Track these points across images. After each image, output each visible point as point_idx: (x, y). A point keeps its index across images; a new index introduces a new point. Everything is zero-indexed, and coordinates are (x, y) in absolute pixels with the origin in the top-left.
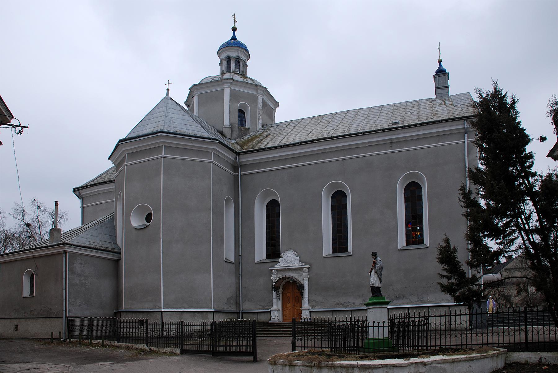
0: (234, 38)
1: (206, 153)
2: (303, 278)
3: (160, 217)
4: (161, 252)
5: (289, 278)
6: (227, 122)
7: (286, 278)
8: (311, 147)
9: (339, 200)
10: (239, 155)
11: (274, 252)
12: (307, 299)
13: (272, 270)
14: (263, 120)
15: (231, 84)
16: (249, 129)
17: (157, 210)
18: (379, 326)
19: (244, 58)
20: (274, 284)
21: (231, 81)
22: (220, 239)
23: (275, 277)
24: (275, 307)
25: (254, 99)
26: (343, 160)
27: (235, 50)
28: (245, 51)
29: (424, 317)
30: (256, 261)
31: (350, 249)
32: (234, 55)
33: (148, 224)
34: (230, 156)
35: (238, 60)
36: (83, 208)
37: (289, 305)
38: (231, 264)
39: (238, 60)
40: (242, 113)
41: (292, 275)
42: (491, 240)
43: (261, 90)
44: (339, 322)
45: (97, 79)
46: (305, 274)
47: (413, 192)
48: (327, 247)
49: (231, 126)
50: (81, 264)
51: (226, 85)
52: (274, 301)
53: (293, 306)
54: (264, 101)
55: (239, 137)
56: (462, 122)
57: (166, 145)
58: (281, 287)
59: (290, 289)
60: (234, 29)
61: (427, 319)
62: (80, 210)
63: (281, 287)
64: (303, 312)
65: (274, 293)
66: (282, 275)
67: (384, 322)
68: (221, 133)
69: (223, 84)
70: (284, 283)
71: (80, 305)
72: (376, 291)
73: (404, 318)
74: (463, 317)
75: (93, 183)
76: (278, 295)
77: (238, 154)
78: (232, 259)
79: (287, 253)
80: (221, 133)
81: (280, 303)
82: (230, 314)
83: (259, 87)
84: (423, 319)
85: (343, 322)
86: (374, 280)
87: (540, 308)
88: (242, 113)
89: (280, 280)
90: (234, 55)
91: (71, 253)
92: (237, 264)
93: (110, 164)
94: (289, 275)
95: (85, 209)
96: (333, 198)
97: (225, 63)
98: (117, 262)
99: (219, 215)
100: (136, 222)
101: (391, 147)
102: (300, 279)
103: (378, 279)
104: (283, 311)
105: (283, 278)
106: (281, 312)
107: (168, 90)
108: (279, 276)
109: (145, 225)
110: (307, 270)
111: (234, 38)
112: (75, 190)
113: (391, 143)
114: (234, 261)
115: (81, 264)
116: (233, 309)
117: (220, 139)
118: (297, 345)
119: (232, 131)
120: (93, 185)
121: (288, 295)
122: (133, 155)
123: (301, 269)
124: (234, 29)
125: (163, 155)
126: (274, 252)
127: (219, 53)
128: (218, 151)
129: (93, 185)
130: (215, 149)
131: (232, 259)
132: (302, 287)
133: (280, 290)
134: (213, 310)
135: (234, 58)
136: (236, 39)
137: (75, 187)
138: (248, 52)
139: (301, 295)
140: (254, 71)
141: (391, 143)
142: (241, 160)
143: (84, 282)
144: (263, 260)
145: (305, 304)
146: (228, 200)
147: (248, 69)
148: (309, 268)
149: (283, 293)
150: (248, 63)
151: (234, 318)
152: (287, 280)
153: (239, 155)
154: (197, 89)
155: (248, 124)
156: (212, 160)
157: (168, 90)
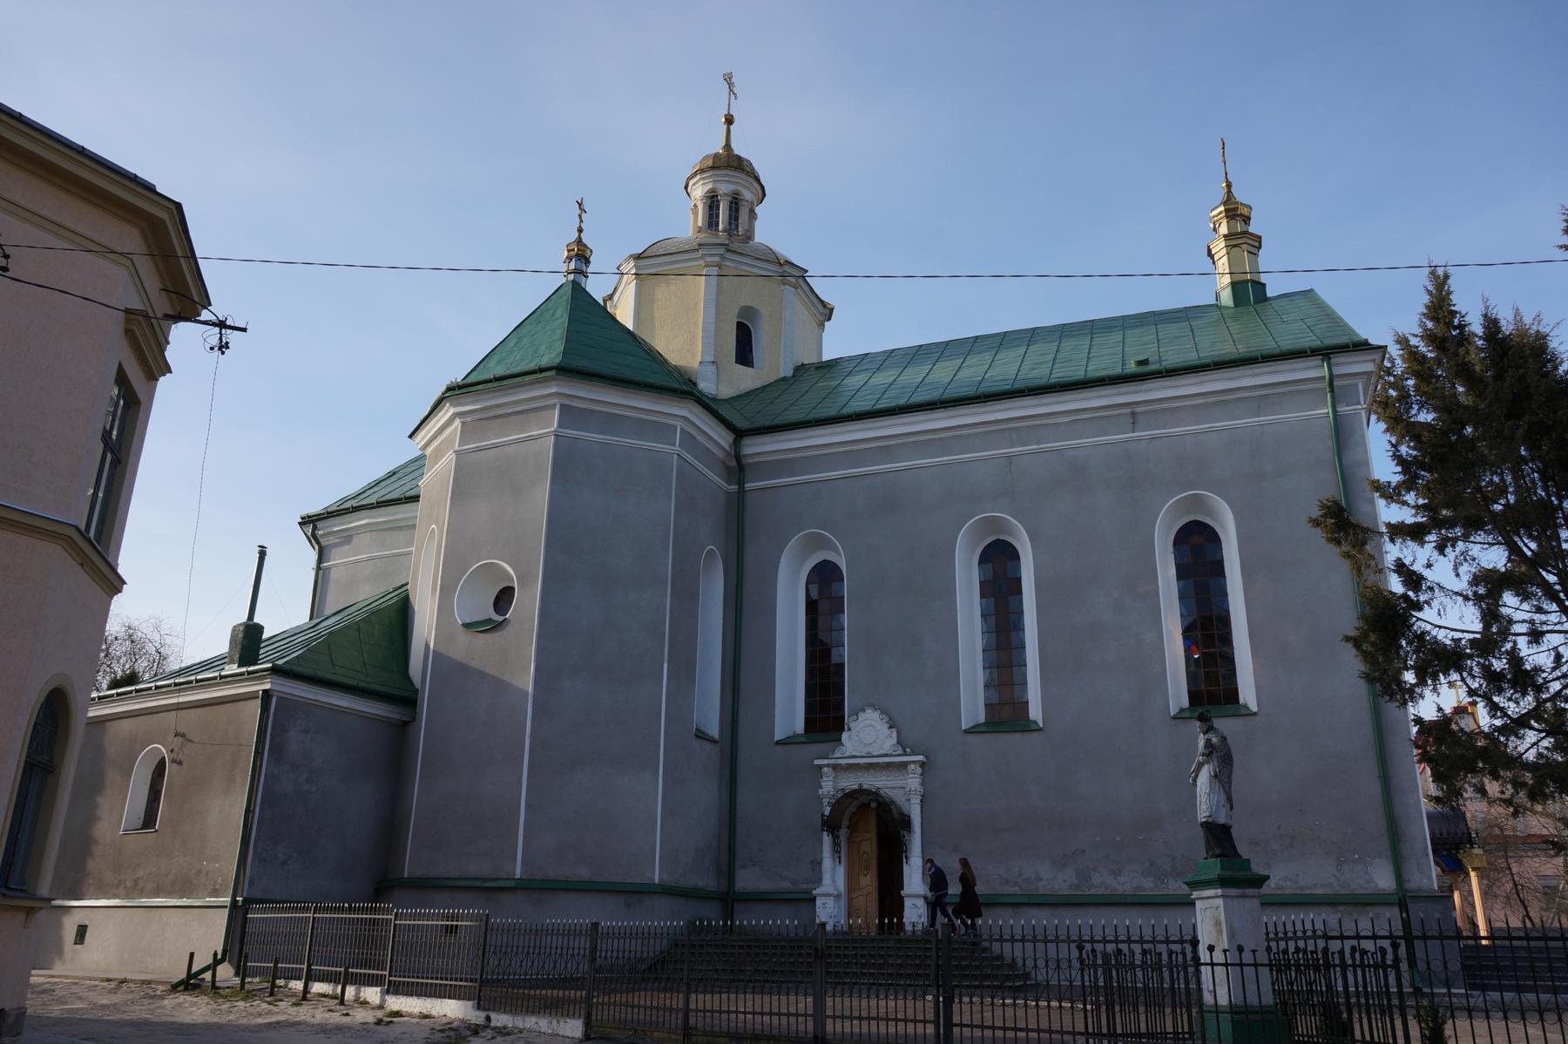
2: (905, 790)
7: (860, 792)
11: (826, 715)
13: (820, 767)
19: (747, 195)
20: (827, 811)
23: (829, 786)
26: (1009, 457)
30: (777, 738)
31: (1248, 693)
33: (501, 618)
34: (723, 438)
41: (878, 784)
42: (1435, 690)
44: (1105, 941)
46: (913, 782)
47: (1198, 549)
48: (972, 704)
52: (827, 862)
56: (1316, 361)
58: (845, 823)
59: (874, 827)
62: (313, 573)
63: (845, 823)
65: (827, 839)
66: (850, 782)
70: (853, 808)
71: (284, 863)
73: (1286, 939)
75: (354, 503)
78: (714, 731)
79: (862, 716)
81: (841, 872)
85: (1116, 941)
92: (730, 743)
96: (984, 559)
98: (401, 733)
99: (687, 597)
101: (1134, 426)
102: (898, 797)
105: (854, 792)
106: (843, 903)
110: (919, 770)
112: (306, 521)
114: (716, 736)
115: (306, 732)
116: (708, 882)
118: (956, 1020)
120: (347, 511)
123: (904, 765)
126: (826, 715)
128: (693, 424)
129: (347, 511)
130: (686, 418)
131: (714, 731)
132: (906, 823)
133: (843, 833)
138: (757, 180)
140: (772, 229)
141: (1134, 416)
143: (306, 787)
144: (795, 736)
147: (757, 224)
148: (922, 764)
149: (849, 839)
150: (758, 210)
151: (711, 915)
152: (864, 799)
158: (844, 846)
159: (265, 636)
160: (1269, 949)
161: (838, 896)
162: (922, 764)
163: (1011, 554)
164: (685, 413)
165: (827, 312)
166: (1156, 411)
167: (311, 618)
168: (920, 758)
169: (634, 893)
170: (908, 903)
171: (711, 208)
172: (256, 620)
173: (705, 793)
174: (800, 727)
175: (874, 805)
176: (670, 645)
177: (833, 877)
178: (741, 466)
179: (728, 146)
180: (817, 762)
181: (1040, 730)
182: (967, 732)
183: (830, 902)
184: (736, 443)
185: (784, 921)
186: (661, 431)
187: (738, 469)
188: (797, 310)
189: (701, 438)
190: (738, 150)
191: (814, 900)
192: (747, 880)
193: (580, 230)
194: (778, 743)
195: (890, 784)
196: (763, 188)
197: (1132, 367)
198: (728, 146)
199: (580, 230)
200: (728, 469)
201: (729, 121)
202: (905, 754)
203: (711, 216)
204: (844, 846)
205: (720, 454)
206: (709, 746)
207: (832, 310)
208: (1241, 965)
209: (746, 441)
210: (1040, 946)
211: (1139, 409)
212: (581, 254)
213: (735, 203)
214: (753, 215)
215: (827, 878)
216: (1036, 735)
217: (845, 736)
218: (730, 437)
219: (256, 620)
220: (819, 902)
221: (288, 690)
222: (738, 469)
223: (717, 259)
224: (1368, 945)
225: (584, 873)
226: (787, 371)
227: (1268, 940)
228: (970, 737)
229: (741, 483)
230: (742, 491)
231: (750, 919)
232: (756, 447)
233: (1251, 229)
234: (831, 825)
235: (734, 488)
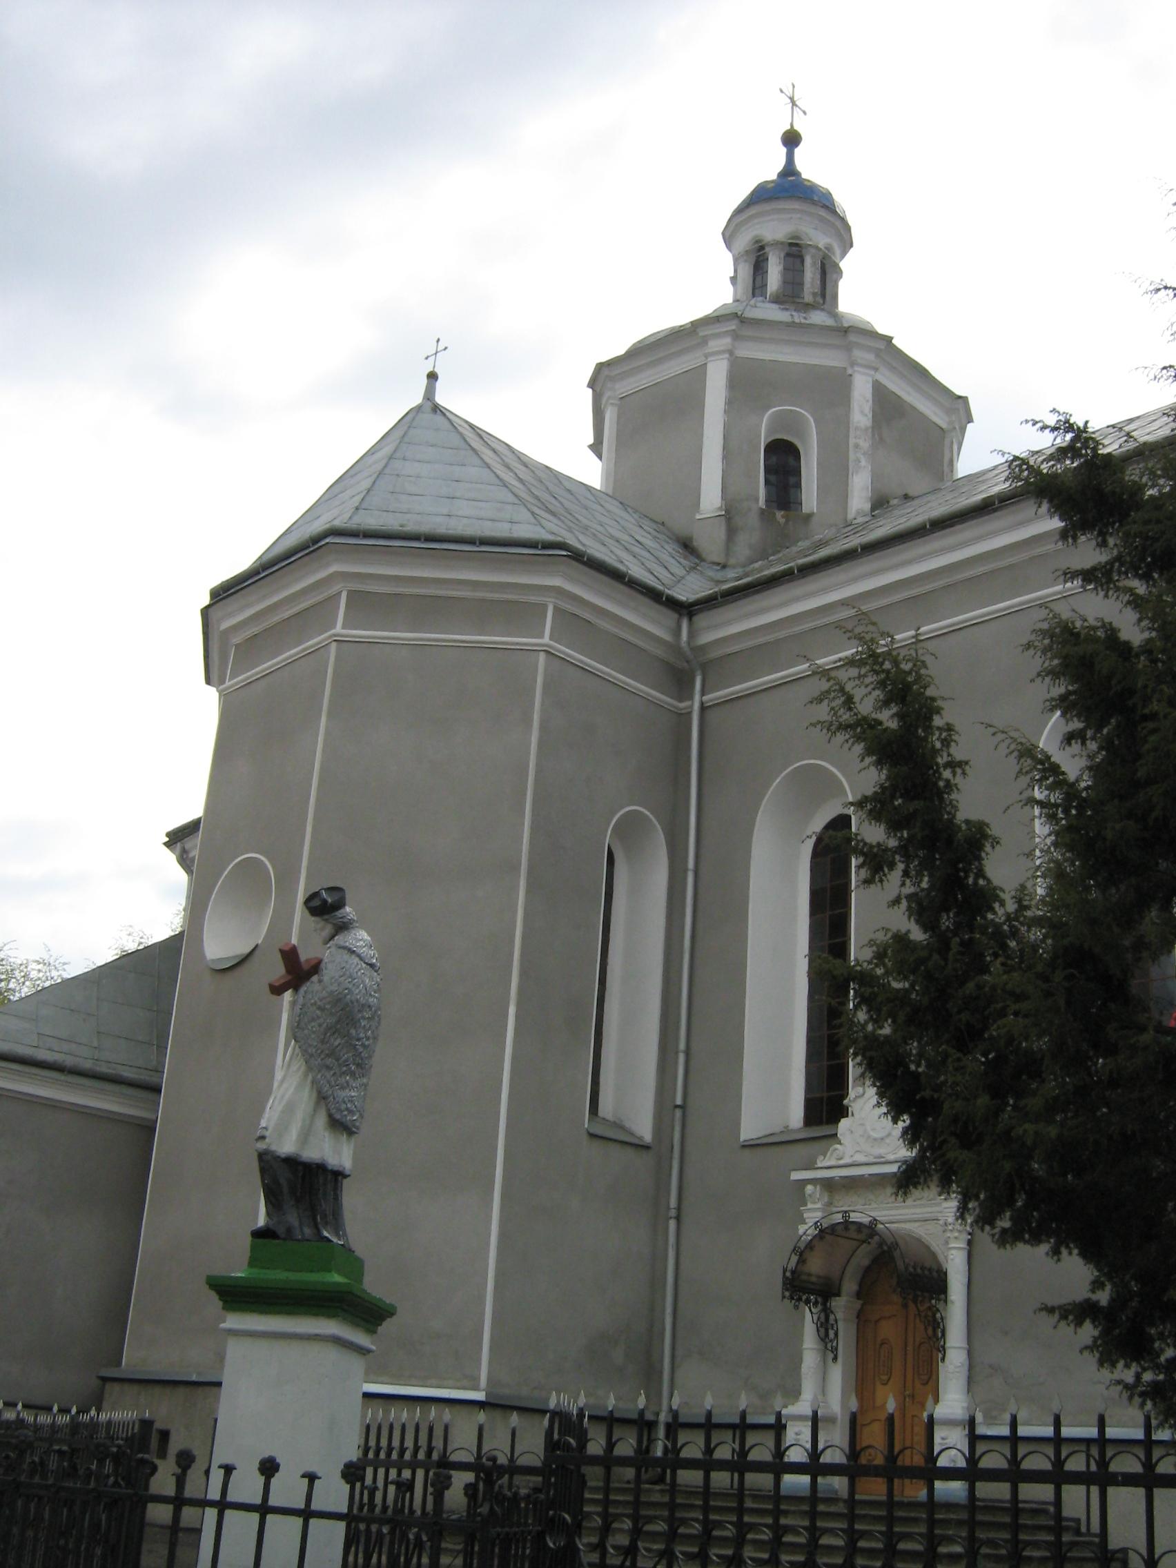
0: (789, 171)
1: (520, 613)
6: (711, 499)
10: (691, 616)
14: (876, 477)
15: (736, 336)
16: (809, 516)
19: (819, 238)
21: (732, 326)
25: (833, 389)
27: (779, 211)
28: (823, 213)
34: (652, 624)
35: (794, 252)
38: (630, 1152)
39: (794, 252)
40: (783, 460)
43: (869, 349)
49: (730, 514)
51: (714, 345)
54: (879, 391)
55: (763, 555)
58: (850, 1286)
60: (791, 140)
67: (269, 1468)
68: (687, 546)
69: (705, 341)
76: (825, 1329)
77: (687, 610)
78: (644, 1129)
80: (687, 546)
83: (852, 337)
87: (94, 1467)
88: (783, 460)
97: (746, 270)
107: (432, 376)
111: (789, 171)
114: (648, 1137)
119: (732, 532)
121: (889, 1330)
122: (252, 649)
124: (791, 140)
125: (338, 629)
127: (729, 236)
130: (559, 591)
131: (644, 1129)
132: (931, 1283)
133: (842, 1306)
134: (479, 1396)
135: (776, 244)
136: (798, 174)
137: (171, 827)
142: (705, 638)
144: (787, 1130)
146: (630, 829)
149: (861, 1318)
153: (691, 616)
154: (612, 379)
155: (810, 495)
156: (546, 639)
157: (432, 376)
164: (556, 582)
180: (796, 1176)
205: (659, 652)
217: (844, 1124)
234: (802, 1287)
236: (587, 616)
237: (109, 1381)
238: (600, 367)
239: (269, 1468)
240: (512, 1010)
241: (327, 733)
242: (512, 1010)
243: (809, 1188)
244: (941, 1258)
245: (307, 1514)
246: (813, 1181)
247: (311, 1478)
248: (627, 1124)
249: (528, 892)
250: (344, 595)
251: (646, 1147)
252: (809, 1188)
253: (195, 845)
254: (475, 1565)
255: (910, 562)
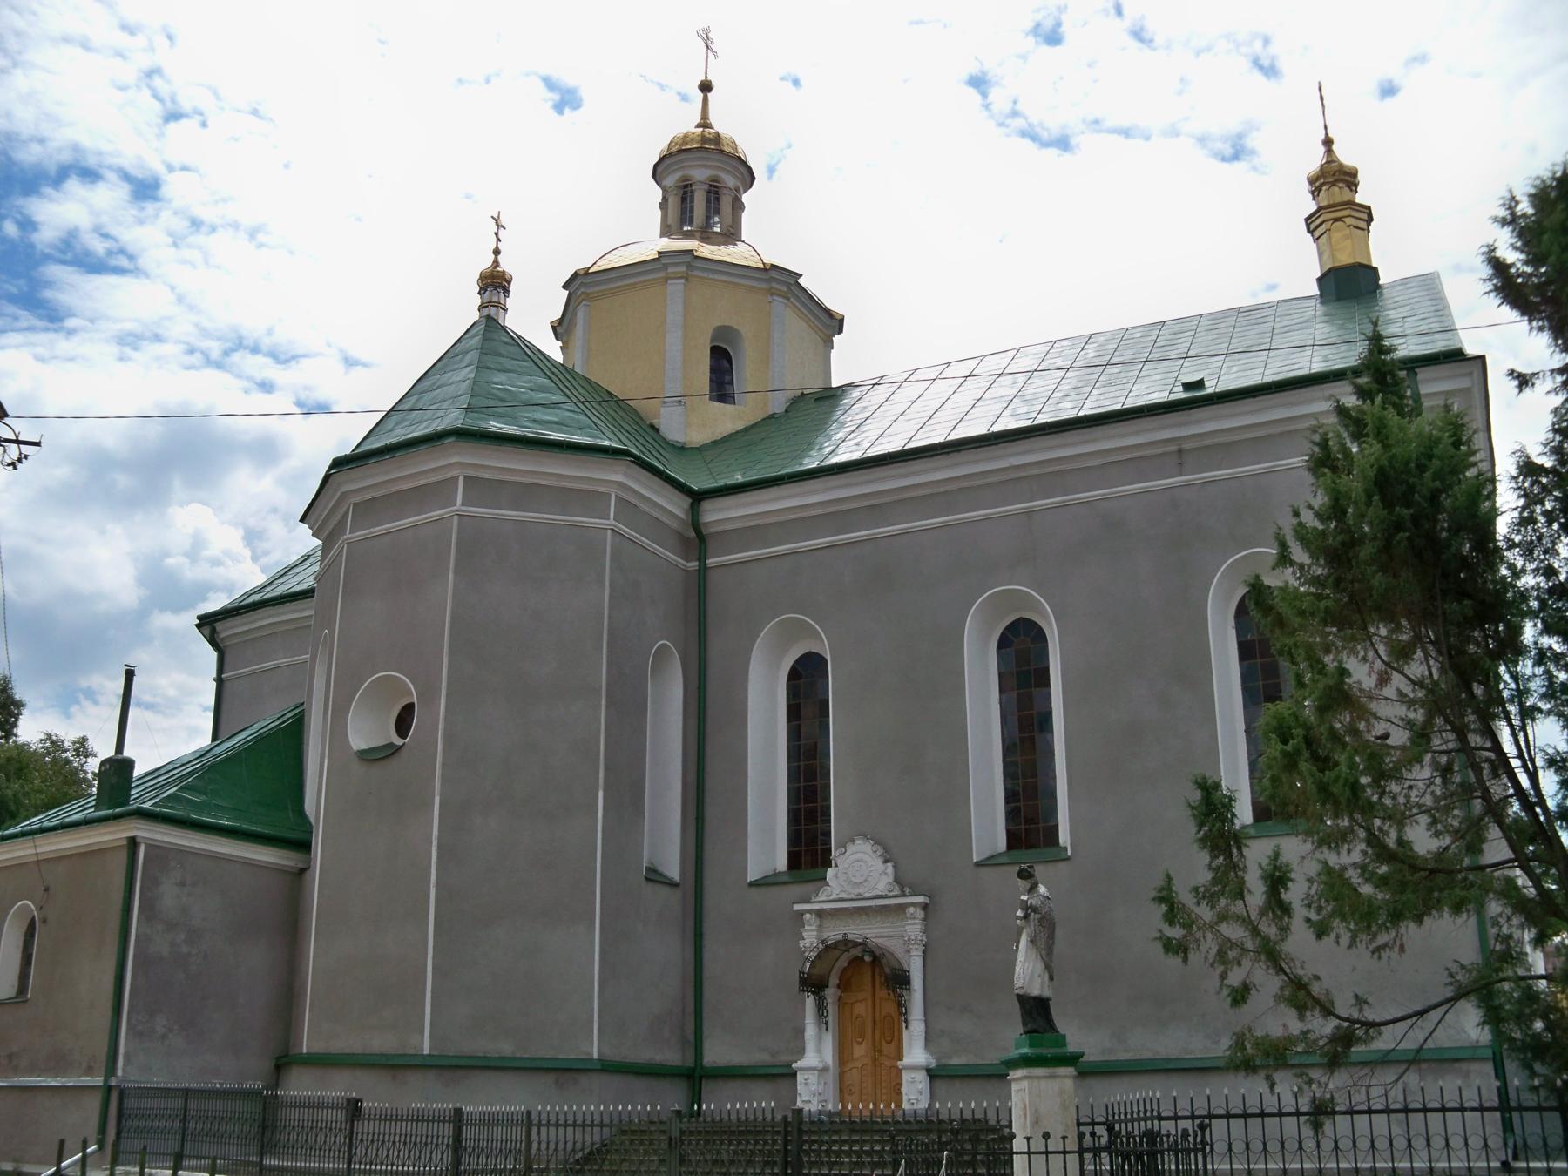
2: (904, 940)
3: (435, 720)
4: (435, 843)
5: (856, 944)
8: (926, 471)
9: (1022, 652)
11: (810, 850)
12: (922, 1026)
13: (802, 913)
17: (428, 693)
18: (1029, 1153)
19: (730, 181)
22: (628, 796)
23: (810, 938)
24: (810, 1059)
26: (1029, 514)
29: (1193, 1117)
31: (1064, 837)
32: (704, 180)
33: (399, 741)
34: (676, 506)
36: (220, 681)
37: (860, 1051)
45: (334, 224)
46: (913, 929)
48: (988, 826)
50: (182, 884)
52: (810, 1031)
53: (877, 1050)
57: (471, 473)
58: (834, 980)
61: (1203, 1127)
63: (834, 980)
64: (906, 1076)
65: (810, 1002)
66: (834, 933)
67: (1046, 1136)
71: (164, 1037)
72: (1036, 1012)
74: (1290, 1122)
75: (256, 598)
76: (821, 1009)
79: (851, 848)
81: (829, 1041)
82: (639, 1084)
84: (1187, 1124)
86: (1027, 972)
89: (829, 950)
90: (704, 180)
91: (155, 849)
93: (306, 540)
94: (856, 930)
95: (227, 685)
96: (1003, 643)
97: (673, 201)
99: (628, 707)
100: (365, 731)
101: (1181, 468)
102: (895, 947)
103: (1040, 966)
104: (842, 1076)
105: (836, 945)
106: (831, 1077)
108: (826, 935)
109: (391, 745)
110: (920, 914)
113: (1180, 451)
115: (182, 884)
116: (672, 1056)
117: (626, 457)
121: (861, 1009)
122: (368, 510)
123: (902, 908)
126: (810, 850)
127: (657, 173)
128: (634, 491)
130: (621, 484)
131: (674, 872)
132: (900, 980)
133: (831, 994)
139: (902, 1008)
141: (1181, 457)
143: (185, 949)
144: (776, 874)
145: (916, 1054)
147: (746, 218)
148: (925, 907)
150: (745, 198)
152: (856, 952)
158: (832, 1009)
159: (137, 773)
160: (1081, 1136)
161: (825, 1069)
162: (925, 907)
163: (1039, 636)
164: (619, 478)
165: (833, 323)
166: (1207, 447)
167: (214, 738)
168: (921, 899)
169: (567, 1071)
170: (906, 1077)
171: (684, 199)
172: (127, 753)
173: (663, 951)
174: (781, 863)
175: (867, 958)
176: (607, 769)
177: (817, 1054)
178: (701, 538)
179: (704, 123)
180: (797, 907)
181: (1068, 859)
182: (978, 864)
183: (813, 1078)
184: (694, 509)
185: (756, 1102)
186: (590, 500)
187: (697, 541)
188: (792, 326)
189: (645, 507)
190: (722, 124)
191: (794, 1075)
192: (716, 1053)
193: (497, 252)
194: (752, 884)
195: (885, 931)
196: (749, 169)
197: (1180, 394)
198: (704, 123)
199: (497, 252)
200: (684, 541)
201: (706, 87)
202: (904, 895)
203: (683, 211)
204: (832, 1009)
205: (674, 525)
206: (664, 891)
207: (842, 321)
208: (1047, 1153)
209: (707, 505)
210: (561, 1130)
211: (1186, 446)
212: (495, 283)
213: (714, 191)
214: (738, 207)
215: (810, 1046)
216: (1061, 865)
217: (830, 872)
218: (686, 502)
219: (127, 753)
220: (800, 1077)
221: (158, 837)
222: (697, 541)
223: (683, 269)
224: (1167, 1126)
225: (506, 1048)
226: (778, 404)
227: (1079, 1124)
228: (984, 871)
229: (702, 559)
230: (703, 569)
231: (724, 1103)
232: (716, 514)
233: (1359, 199)
234: (813, 984)
235: (694, 565)
236: (633, 501)
237: (283, 1062)
238: (576, 275)
239: (1046, 1136)
240: (601, 794)
241: (455, 586)
242: (601, 794)
243: (807, 916)
244: (903, 962)
245: (1065, 1153)
246: (810, 911)
247: (1064, 1138)
248: (660, 869)
249: (607, 707)
250: (461, 479)
251: (673, 885)
252: (807, 916)
253: (225, 629)
254: (1563, 1165)
255: (861, 484)
